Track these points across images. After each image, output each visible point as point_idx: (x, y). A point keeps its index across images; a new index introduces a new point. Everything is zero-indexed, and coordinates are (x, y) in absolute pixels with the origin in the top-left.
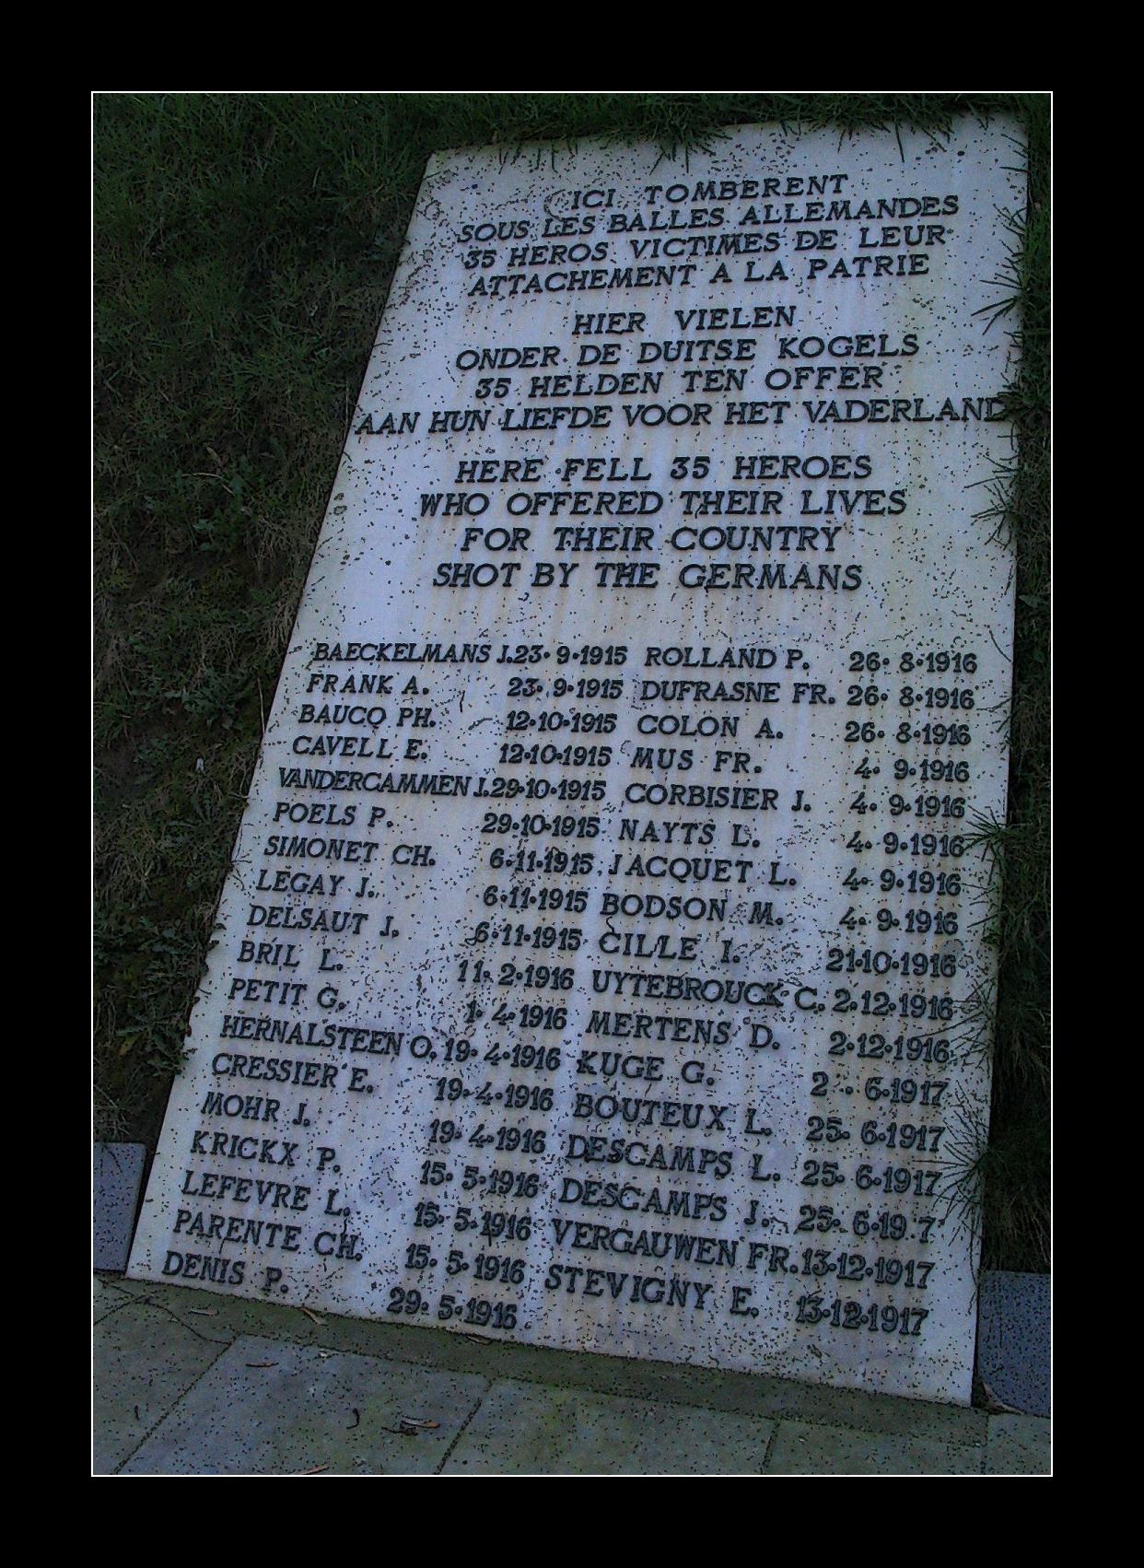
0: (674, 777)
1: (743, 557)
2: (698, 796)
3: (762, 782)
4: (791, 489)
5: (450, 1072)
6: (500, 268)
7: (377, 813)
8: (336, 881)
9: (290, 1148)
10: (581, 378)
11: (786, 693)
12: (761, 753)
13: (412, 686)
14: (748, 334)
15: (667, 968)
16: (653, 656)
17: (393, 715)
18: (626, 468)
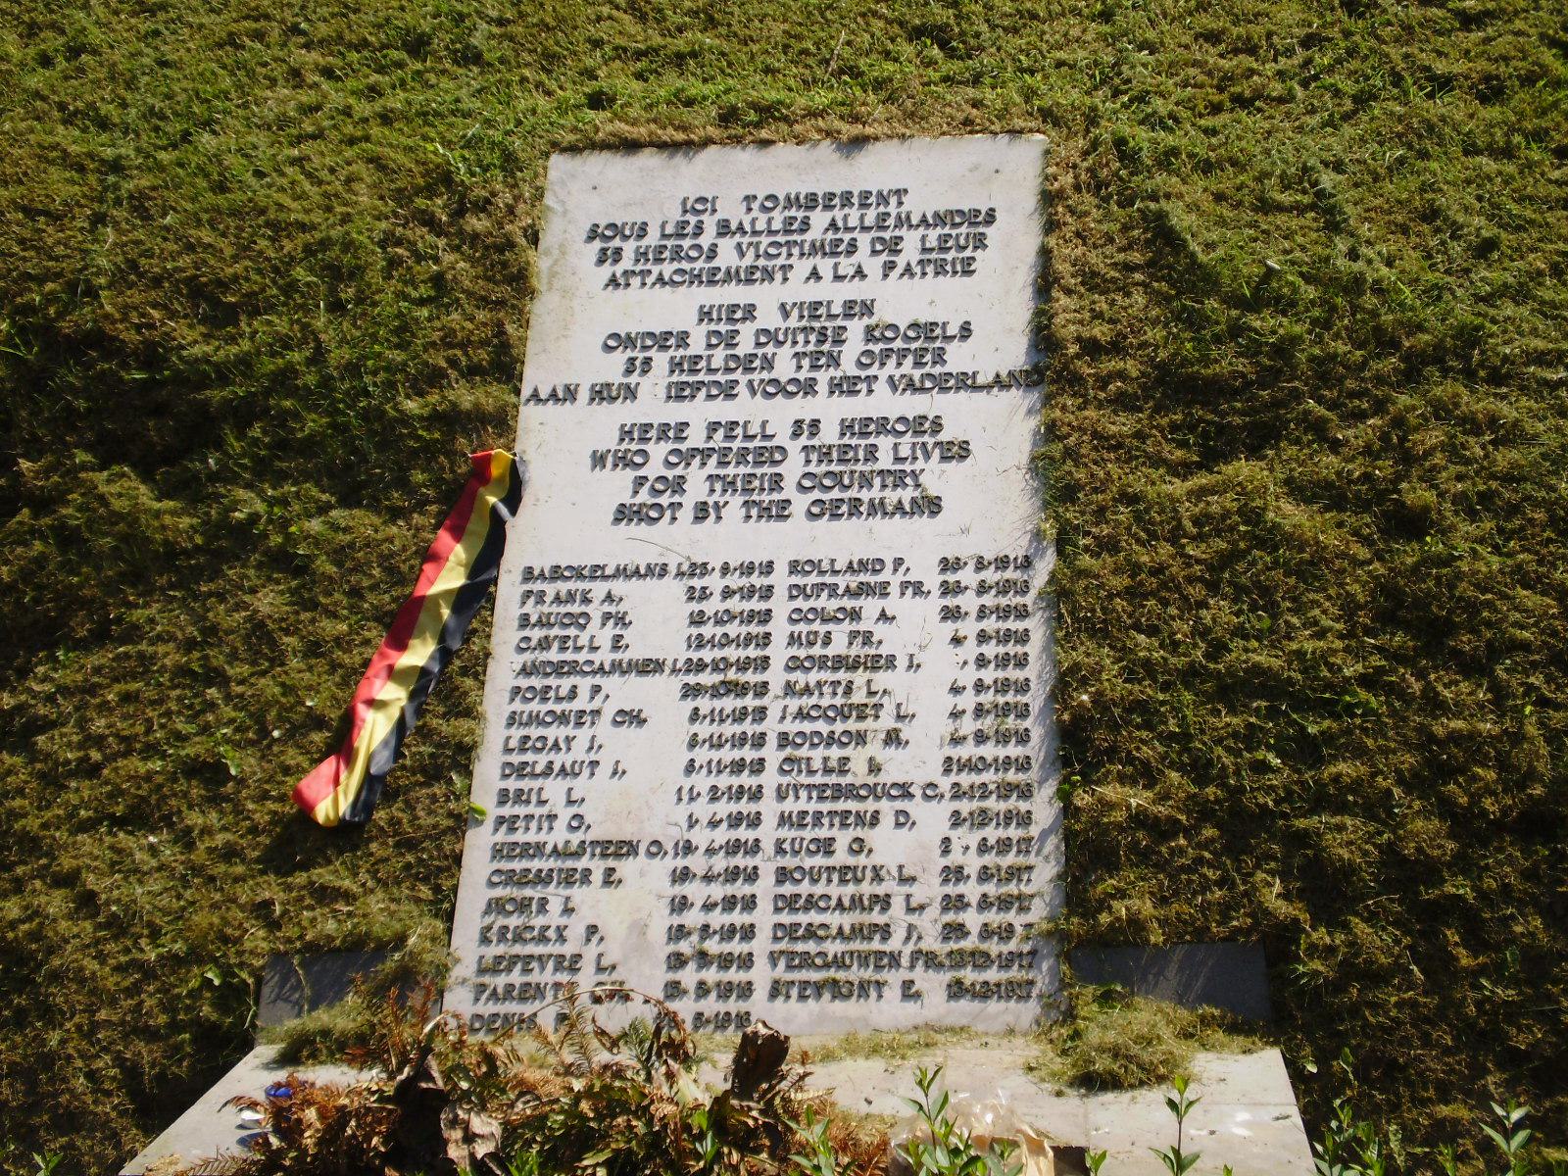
0: (817, 650)
1: (853, 493)
2: (840, 662)
3: (884, 651)
4: (885, 443)
5: (680, 863)
6: (627, 262)
7: (597, 689)
8: (569, 740)
9: (560, 930)
10: (710, 357)
11: (894, 590)
12: (880, 631)
13: (609, 598)
14: (839, 322)
15: (833, 779)
16: (795, 567)
17: (596, 619)
18: (754, 429)
